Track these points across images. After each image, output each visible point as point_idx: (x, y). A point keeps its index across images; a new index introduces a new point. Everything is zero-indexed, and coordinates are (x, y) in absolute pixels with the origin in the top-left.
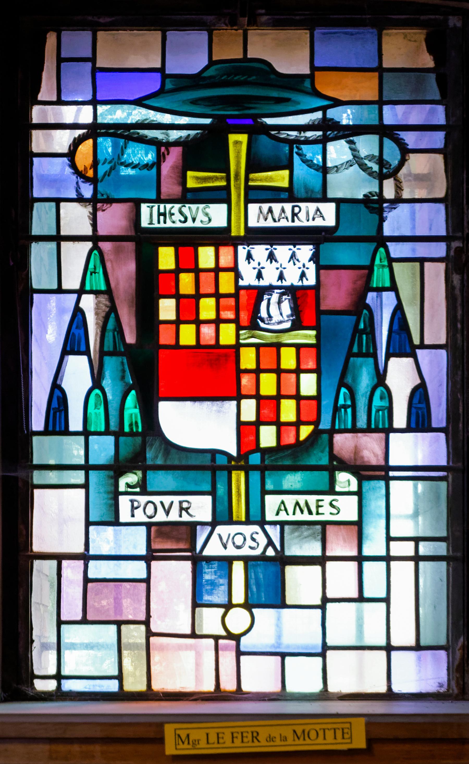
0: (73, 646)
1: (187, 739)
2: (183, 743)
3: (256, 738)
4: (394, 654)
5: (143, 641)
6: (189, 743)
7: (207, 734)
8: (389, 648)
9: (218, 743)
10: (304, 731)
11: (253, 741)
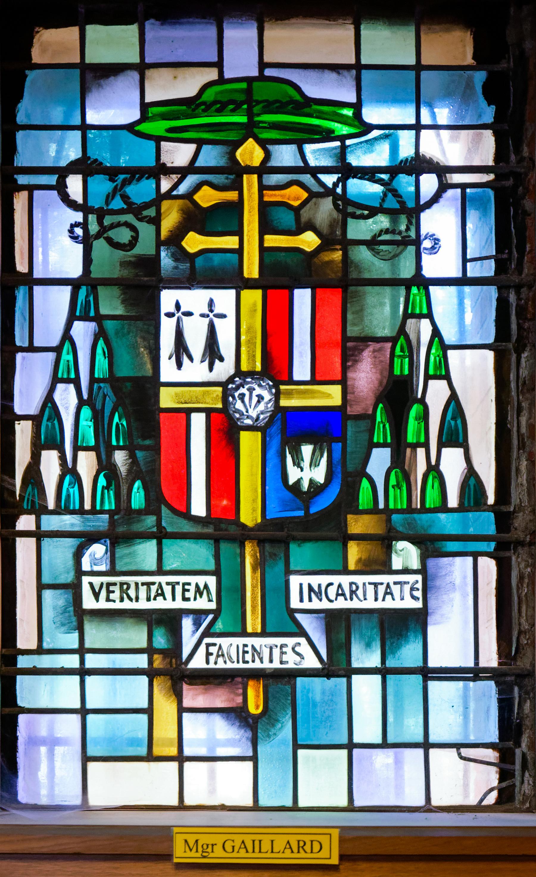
0: (398, 762)
1: (187, 845)
2: (191, 850)
3: (302, 847)
4: (433, 752)
5: (391, 752)
6: (197, 851)
7: (272, 841)
8: (426, 745)
9: (272, 852)
10: (197, 841)
11: (299, 852)
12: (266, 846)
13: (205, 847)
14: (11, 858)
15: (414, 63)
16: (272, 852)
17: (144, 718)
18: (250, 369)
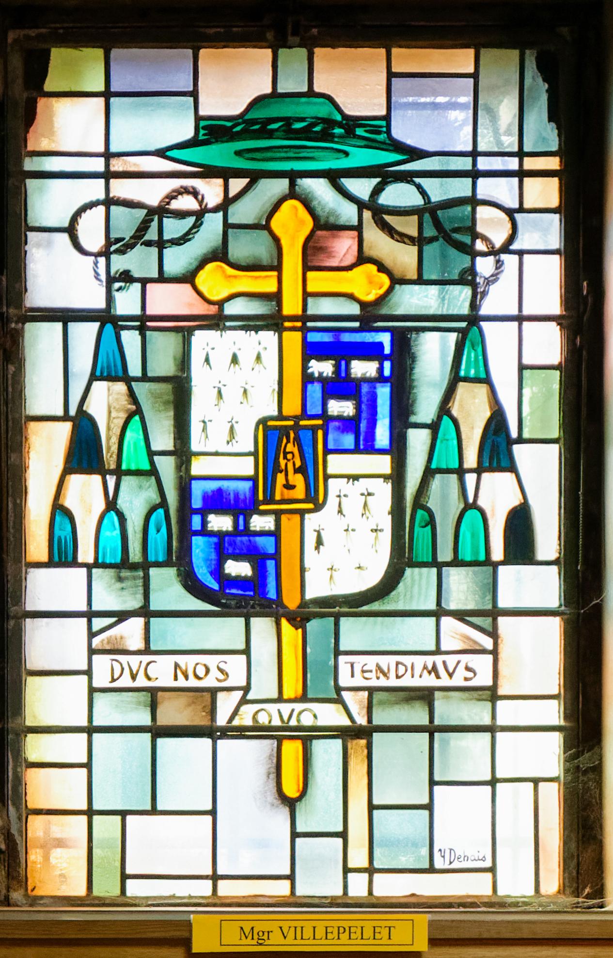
7: (314, 928)
10: (252, 928)
12: (320, 933)
13: (261, 934)
14: (547, 945)
15: (69, 324)
16: (362, 939)
17: (299, 829)
18: (474, 559)
